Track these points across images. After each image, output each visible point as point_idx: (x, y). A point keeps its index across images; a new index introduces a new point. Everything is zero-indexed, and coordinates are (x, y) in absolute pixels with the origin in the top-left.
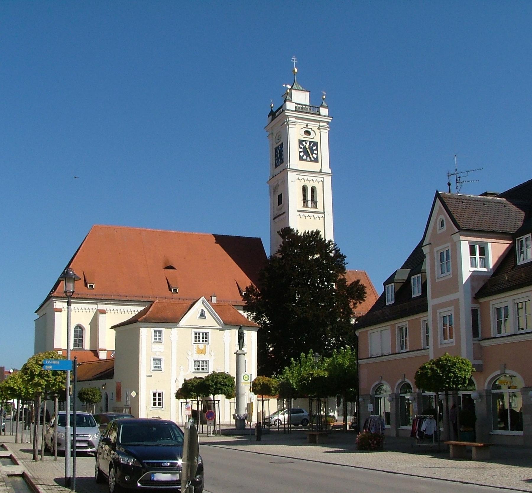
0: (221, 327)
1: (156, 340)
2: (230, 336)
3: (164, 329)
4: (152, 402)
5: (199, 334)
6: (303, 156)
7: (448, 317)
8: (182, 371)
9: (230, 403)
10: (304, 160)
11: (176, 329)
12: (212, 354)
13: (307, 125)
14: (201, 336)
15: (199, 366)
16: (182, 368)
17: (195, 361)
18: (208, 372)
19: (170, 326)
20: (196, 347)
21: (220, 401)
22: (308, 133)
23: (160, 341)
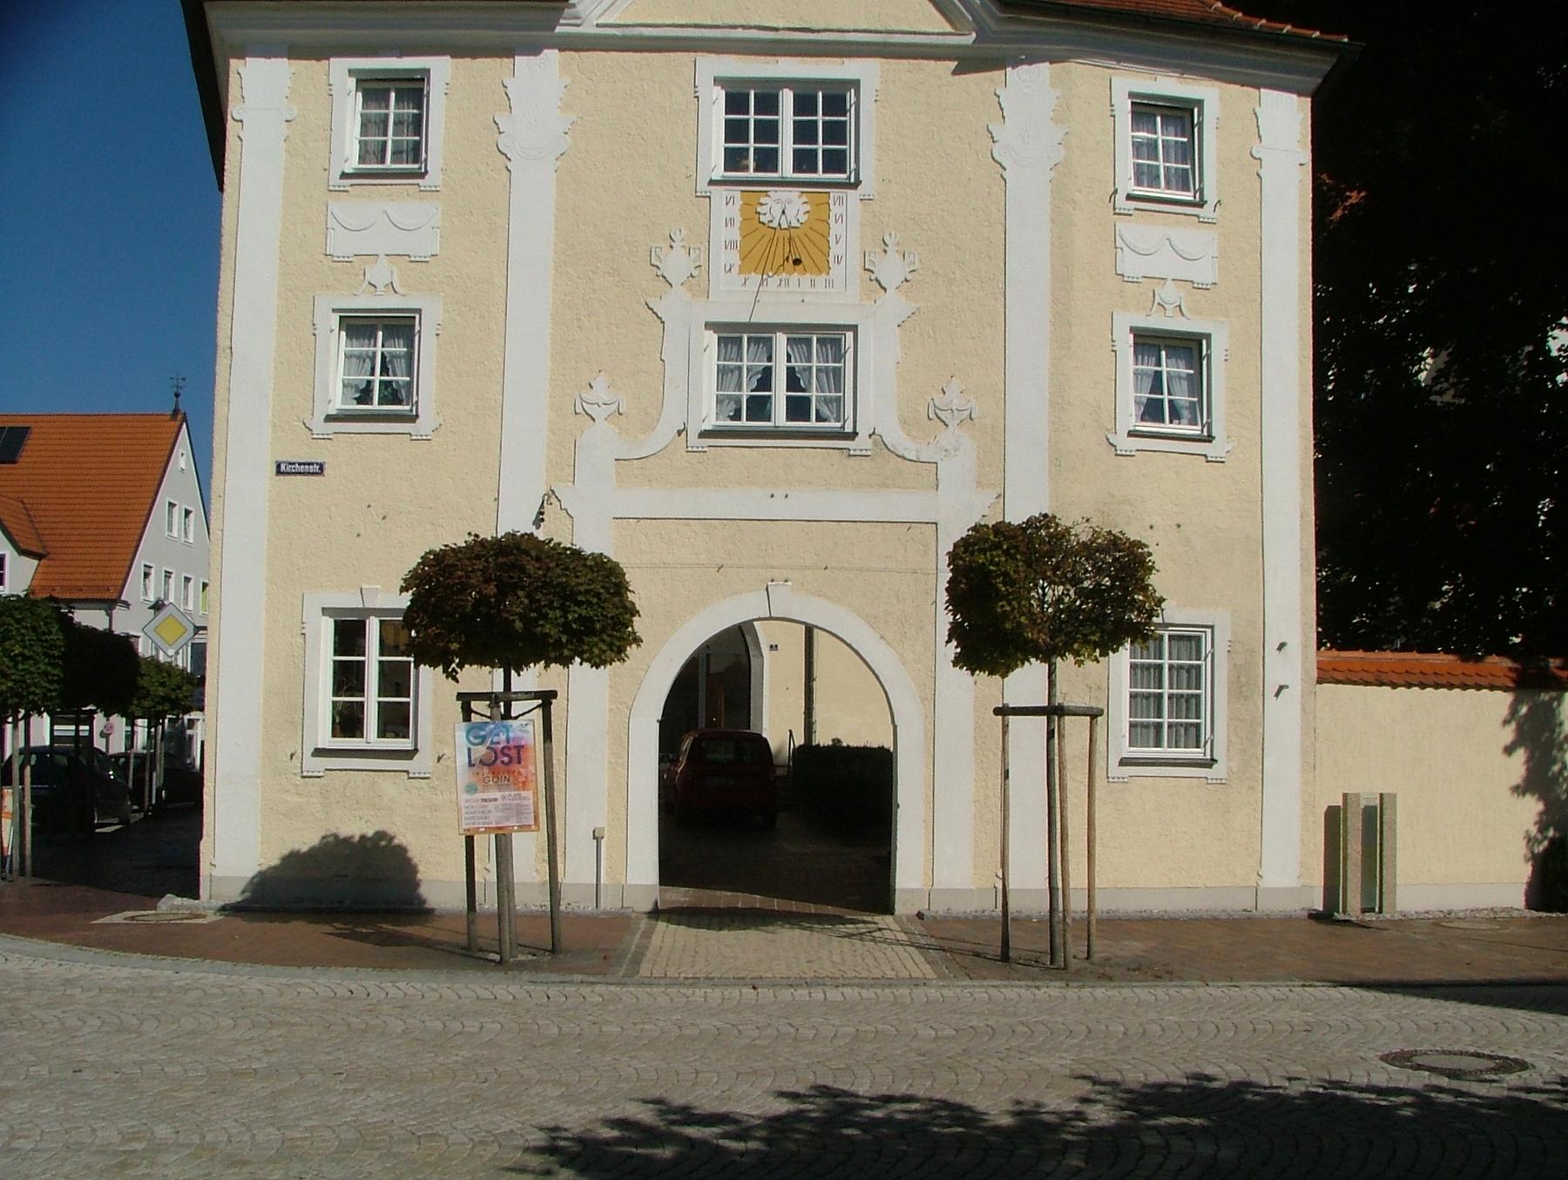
0: (969, 39)
1: (1154, 181)
2: (1056, 120)
3: (446, 60)
4: (323, 699)
5: (768, 103)
8: (601, 425)
9: (1003, 711)
11: (551, 55)
12: (891, 269)
14: (787, 118)
15: (765, 380)
16: (601, 392)
17: (730, 336)
18: (853, 436)
19: (491, 35)
20: (735, 211)
21: (553, 694)
23: (1187, 196)
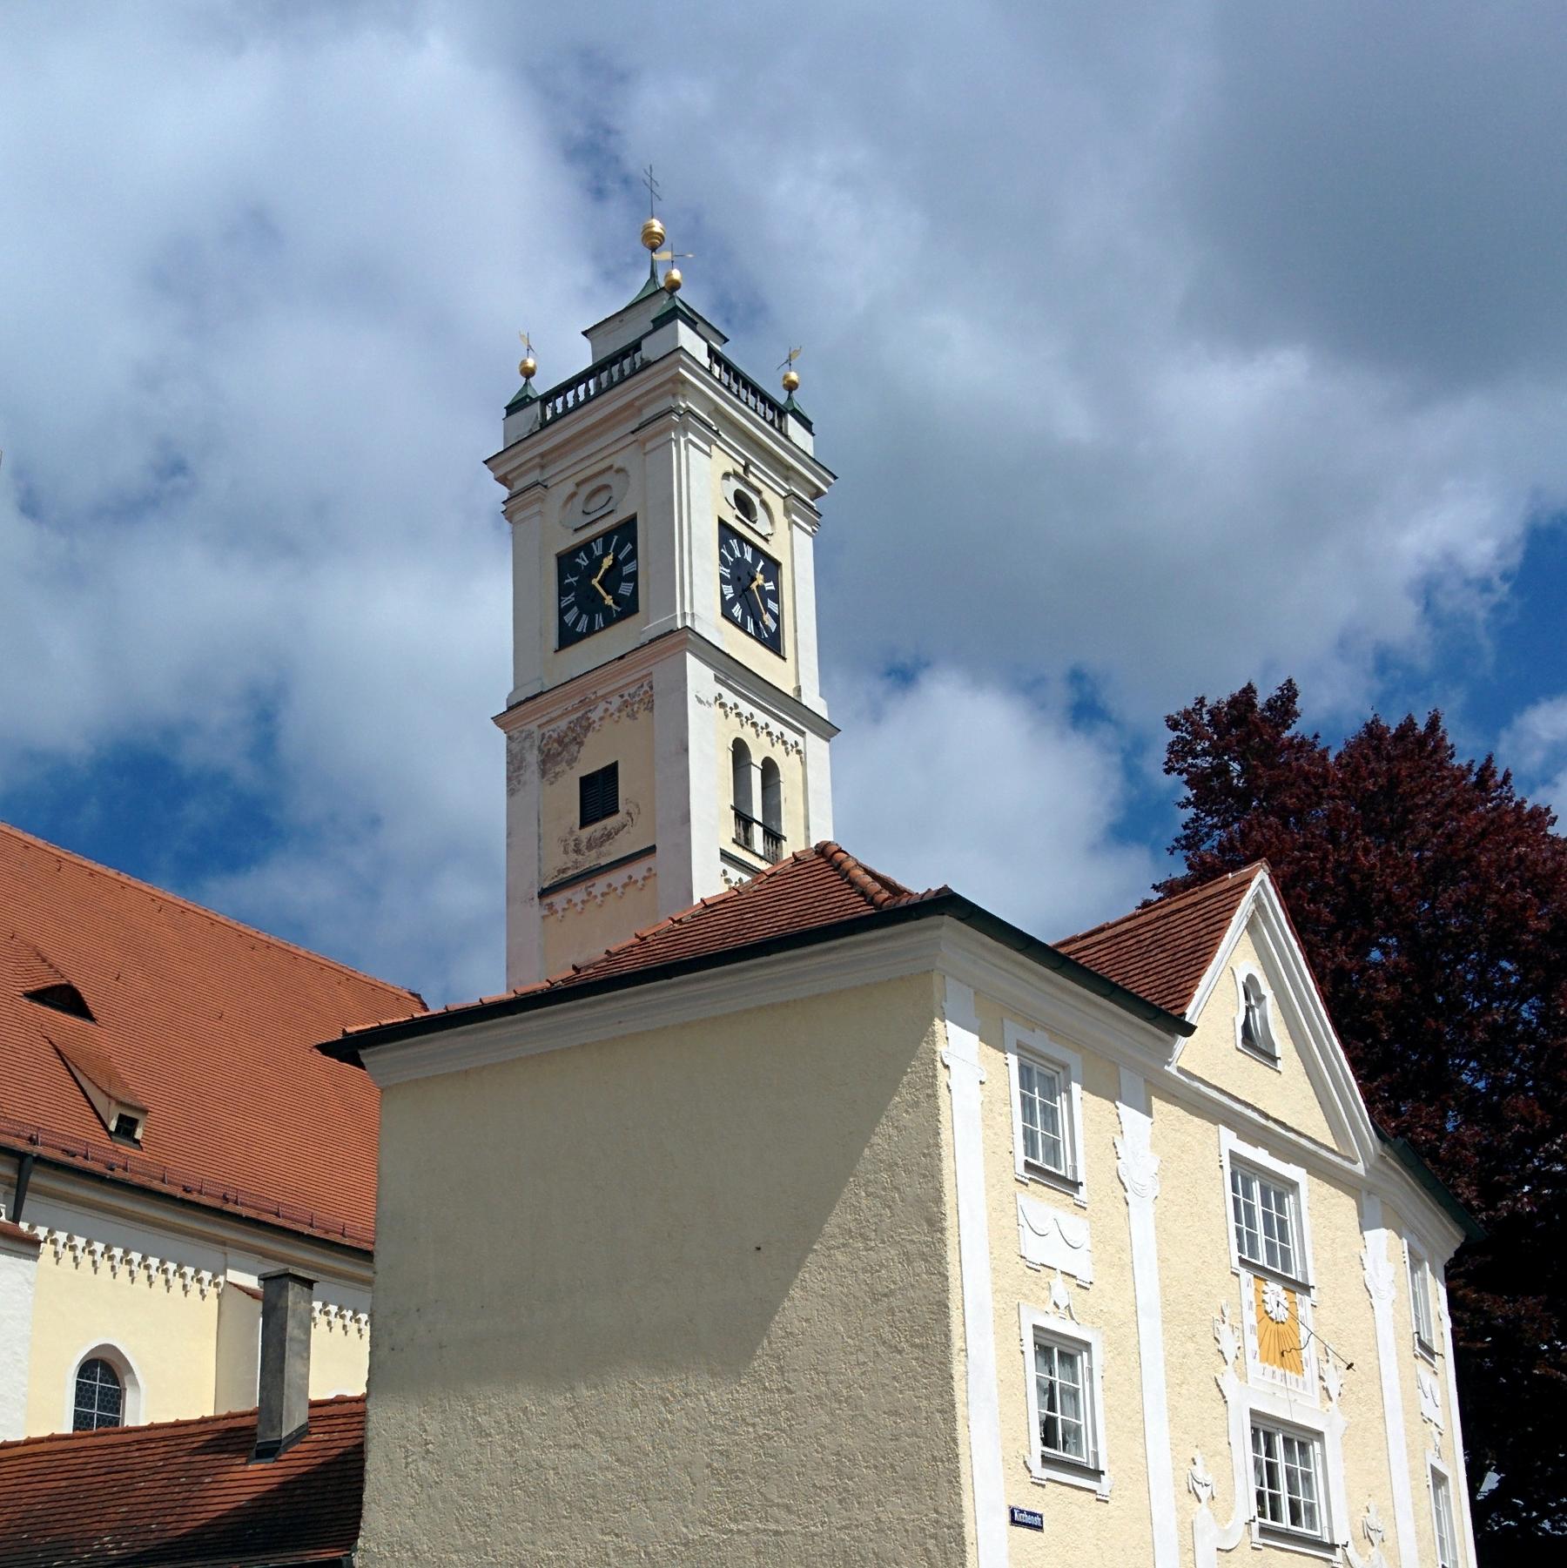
10: (581, 637)
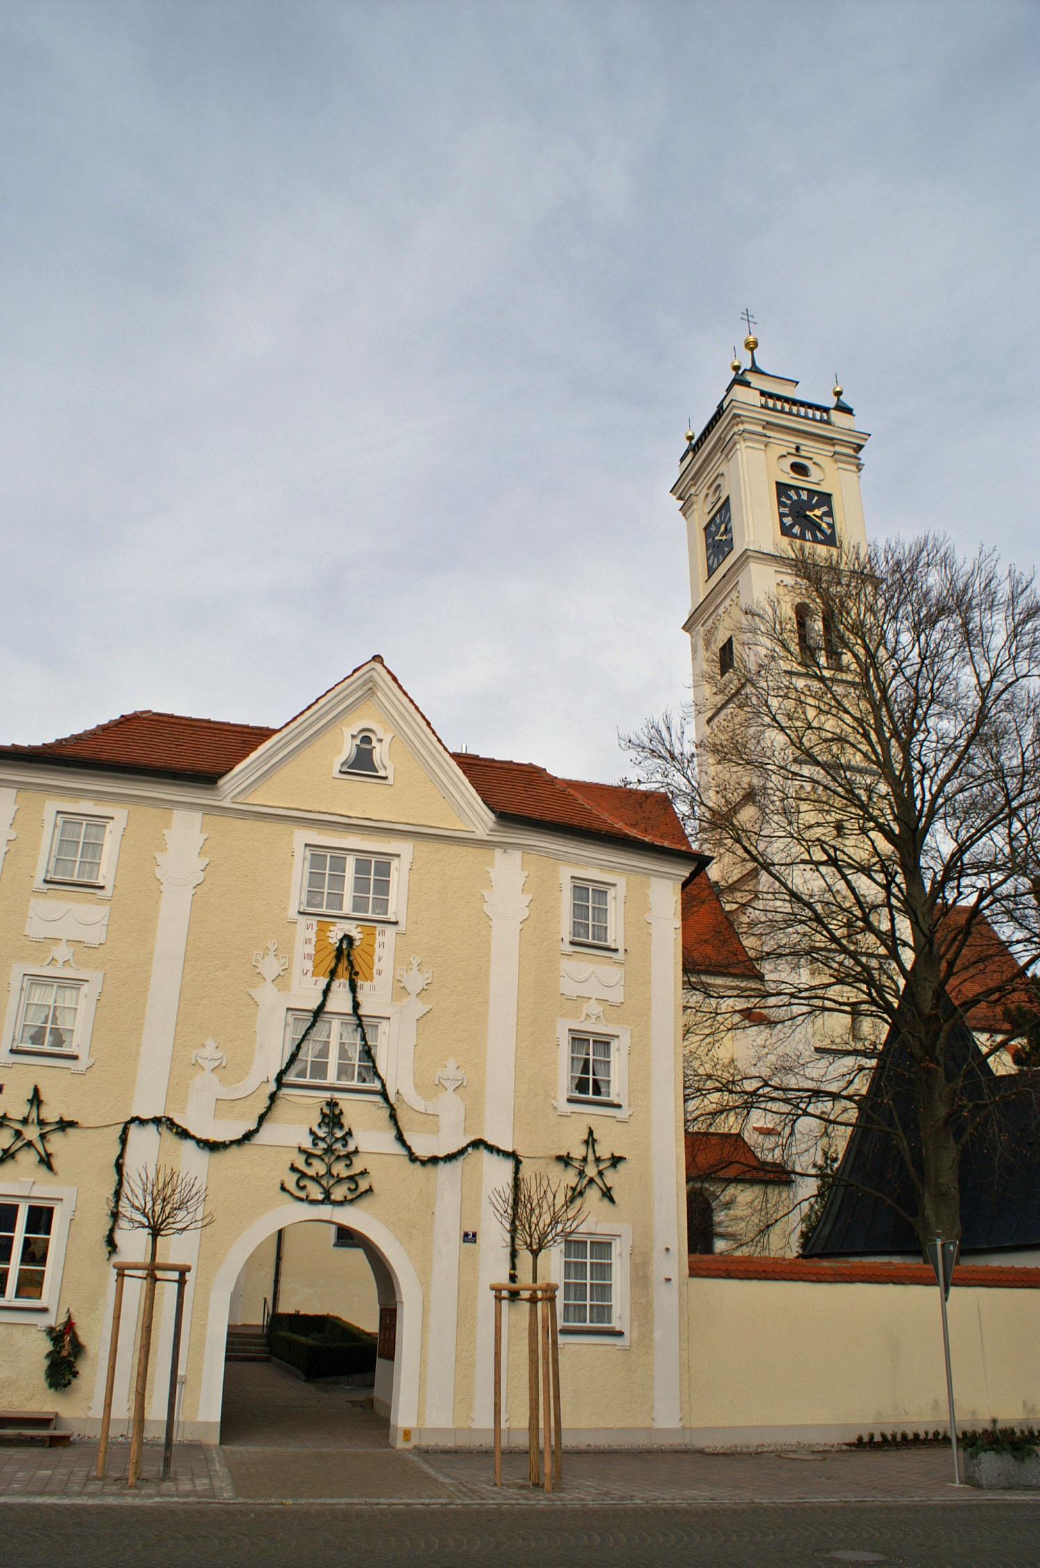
5: (339, 864)
6: (792, 526)
7: (607, 1079)
13: (798, 449)
20: (312, 934)
22: (799, 469)
